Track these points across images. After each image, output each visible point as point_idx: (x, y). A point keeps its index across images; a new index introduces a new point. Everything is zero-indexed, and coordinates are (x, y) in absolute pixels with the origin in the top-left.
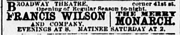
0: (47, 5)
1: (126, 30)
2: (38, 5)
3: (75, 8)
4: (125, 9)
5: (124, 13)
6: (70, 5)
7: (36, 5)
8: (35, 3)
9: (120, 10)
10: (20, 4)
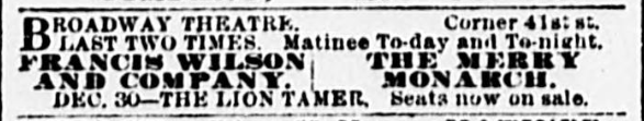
0: (164, 28)
1: (97, 106)
2: (132, 29)
3: (60, 21)
4: (396, 43)
5: (396, 56)
6: (235, 30)
7: (124, 29)
8: (118, 23)
9: (375, 47)
10: (66, 25)
